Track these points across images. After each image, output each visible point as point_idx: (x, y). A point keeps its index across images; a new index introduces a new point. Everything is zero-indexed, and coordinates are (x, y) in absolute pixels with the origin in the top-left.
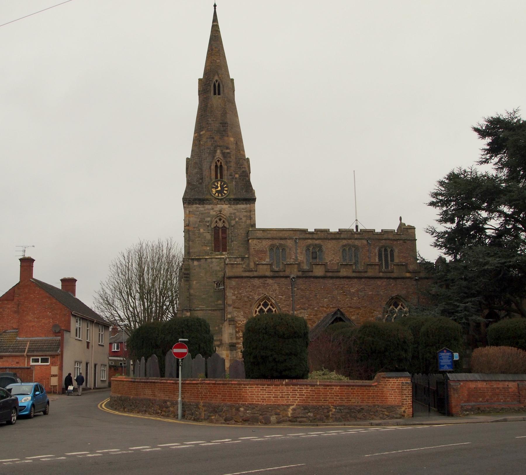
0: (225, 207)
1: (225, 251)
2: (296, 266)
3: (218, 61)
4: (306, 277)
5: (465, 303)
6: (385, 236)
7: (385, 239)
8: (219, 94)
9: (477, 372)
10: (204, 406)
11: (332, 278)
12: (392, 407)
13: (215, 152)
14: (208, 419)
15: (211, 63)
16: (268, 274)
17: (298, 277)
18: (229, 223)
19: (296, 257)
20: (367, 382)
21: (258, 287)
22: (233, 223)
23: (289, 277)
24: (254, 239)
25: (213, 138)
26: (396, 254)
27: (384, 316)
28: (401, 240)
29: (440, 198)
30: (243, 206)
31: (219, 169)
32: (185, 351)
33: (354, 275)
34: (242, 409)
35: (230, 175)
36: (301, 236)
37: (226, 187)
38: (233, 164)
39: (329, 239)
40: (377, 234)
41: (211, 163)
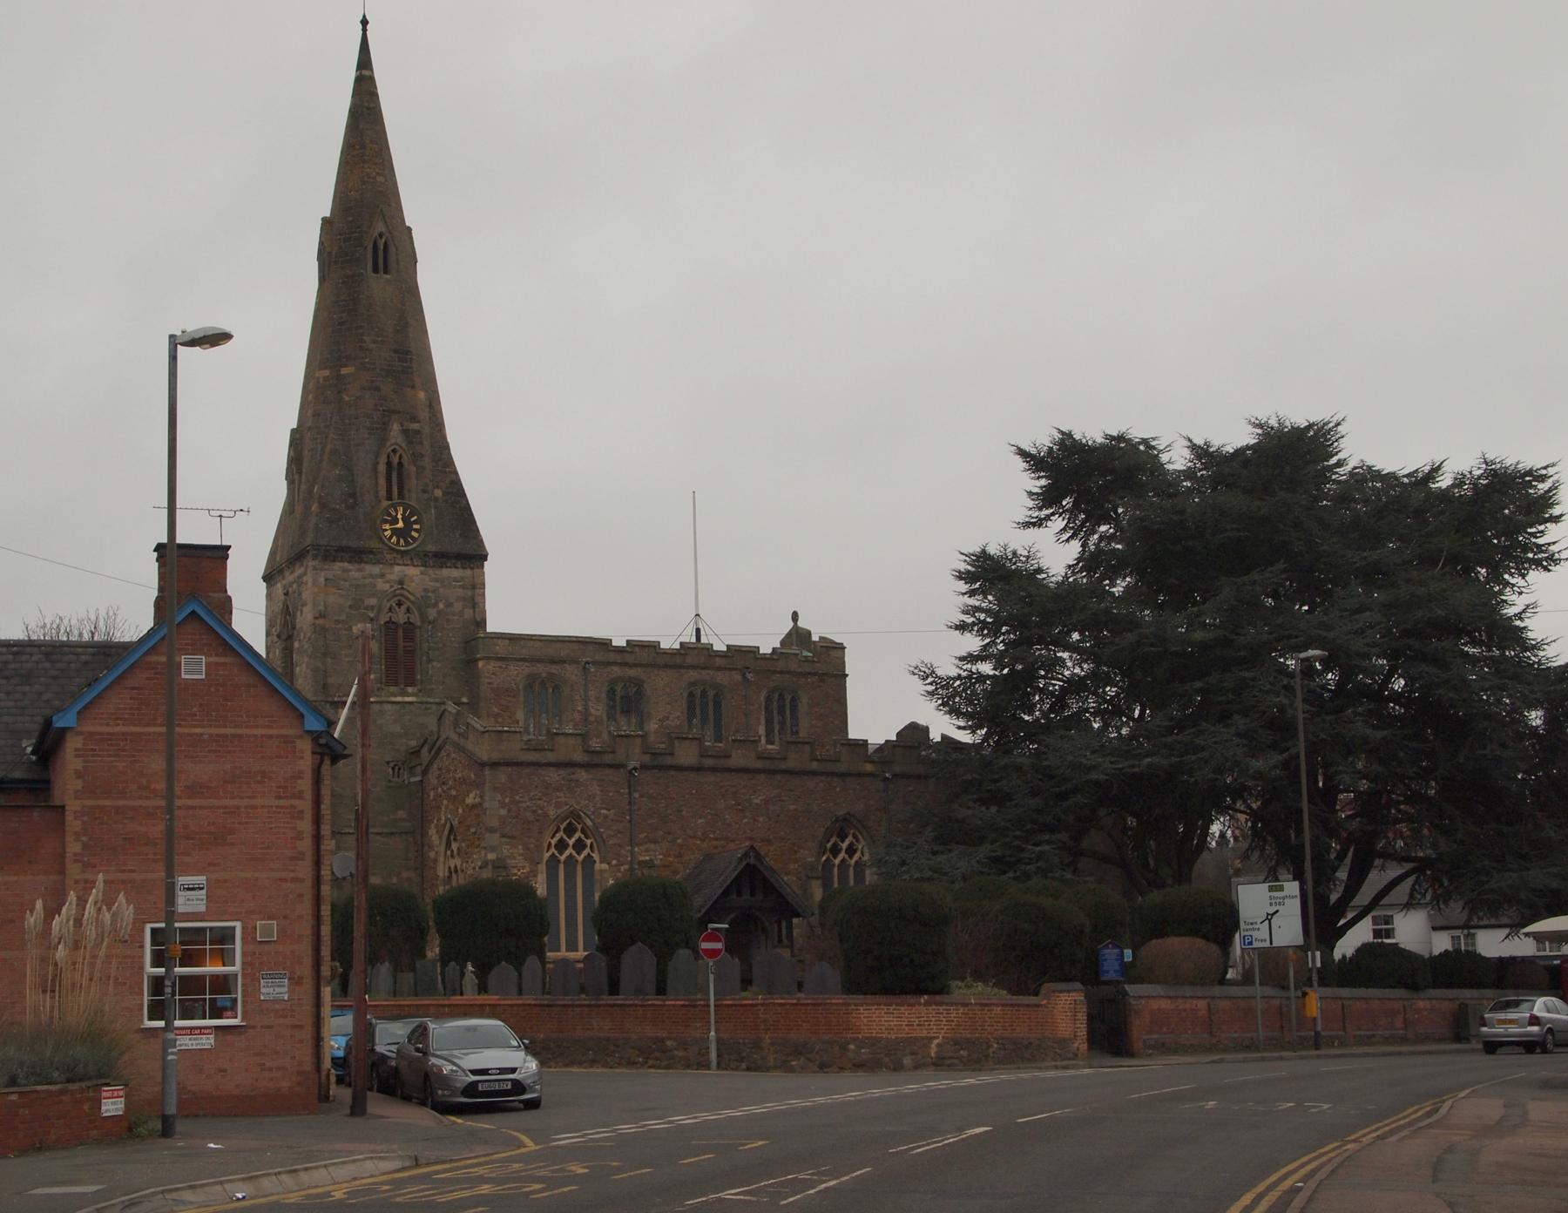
0: (413, 571)
1: (412, 684)
2: (638, 741)
3: (380, 179)
4: (660, 768)
5: (1036, 845)
6: (781, 665)
7: (781, 672)
8: (386, 272)
9: (1159, 982)
10: (772, 1044)
11: (714, 770)
12: (1064, 1040)
13: (385, 426)
14: (785, 1067)
15: (364, 183)
16: (578, 757)
17: (644, 767)
18: (423, 616)
19: (586, 708)
20: (1033, 1000)
21: (557, 789)
22: (432, 613)
23: (623, 766)
24: (488, 658)
25: (377, 389)
26: (803, 707)
27: (818, 859)
28: (815, 674)
29: (982, 616)
30: (455, 573)
31: (396, 472)
32: (719, 945)
33: (759, 764)
34: (852, 1047)
35: (425, 491)
36: (598, 657)
37: (416, 522)
38: (427, 462)
39: (659, 667)
40: (764, 657)
41: (377, 455)
